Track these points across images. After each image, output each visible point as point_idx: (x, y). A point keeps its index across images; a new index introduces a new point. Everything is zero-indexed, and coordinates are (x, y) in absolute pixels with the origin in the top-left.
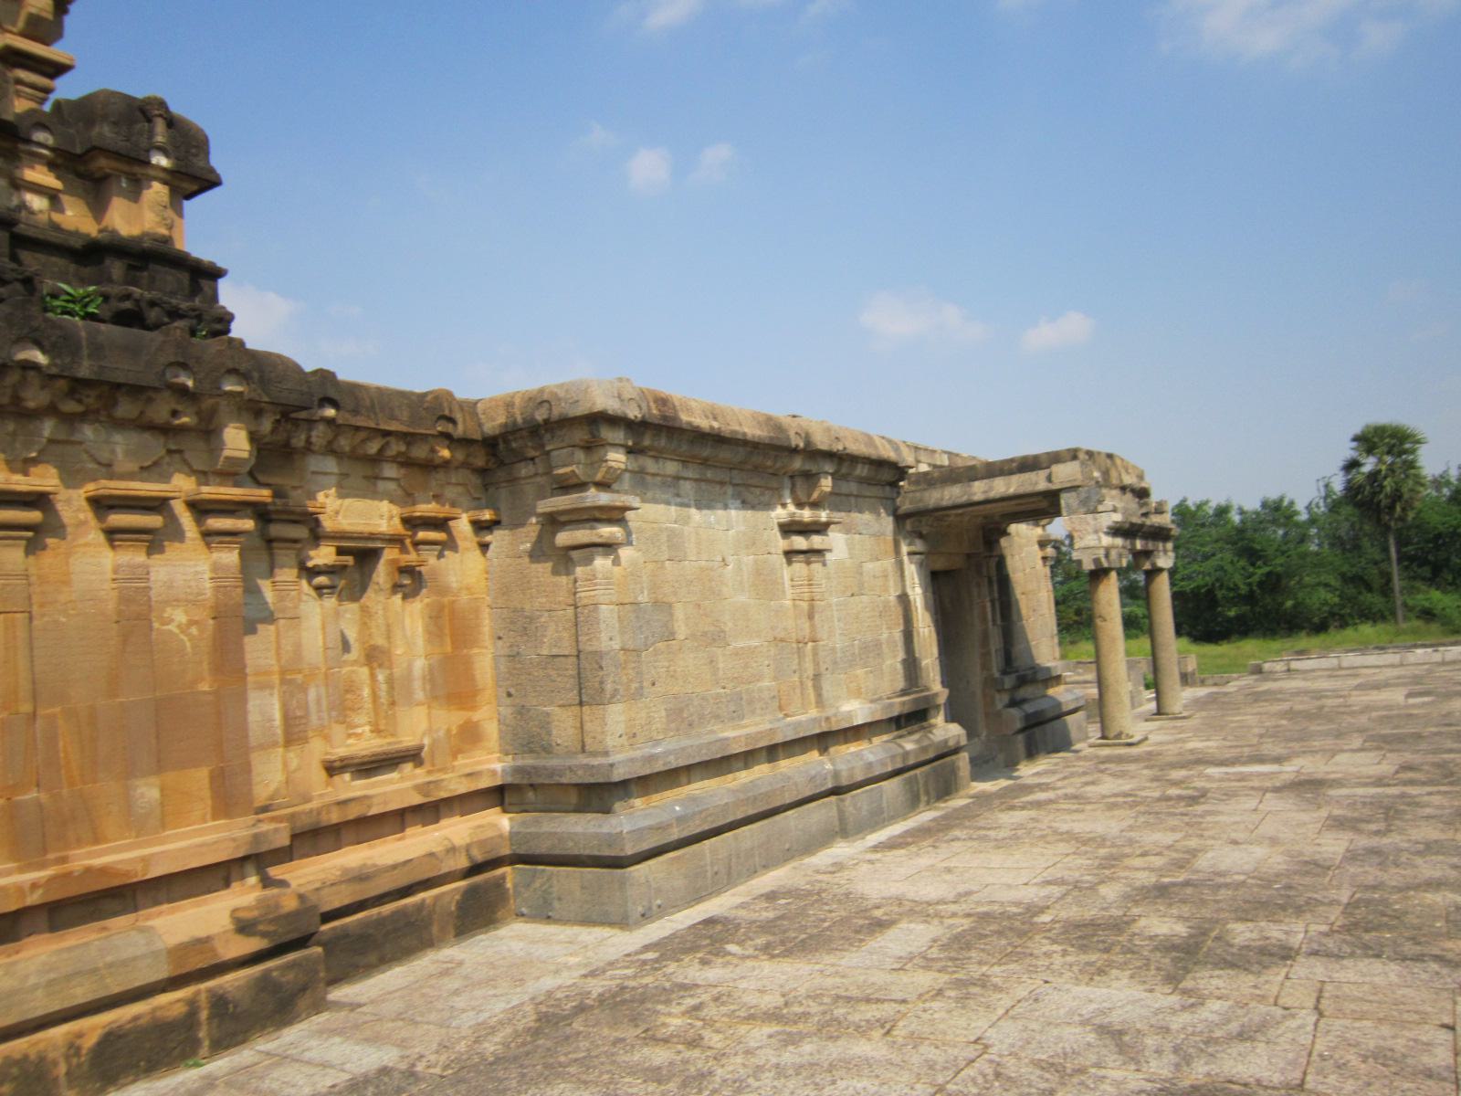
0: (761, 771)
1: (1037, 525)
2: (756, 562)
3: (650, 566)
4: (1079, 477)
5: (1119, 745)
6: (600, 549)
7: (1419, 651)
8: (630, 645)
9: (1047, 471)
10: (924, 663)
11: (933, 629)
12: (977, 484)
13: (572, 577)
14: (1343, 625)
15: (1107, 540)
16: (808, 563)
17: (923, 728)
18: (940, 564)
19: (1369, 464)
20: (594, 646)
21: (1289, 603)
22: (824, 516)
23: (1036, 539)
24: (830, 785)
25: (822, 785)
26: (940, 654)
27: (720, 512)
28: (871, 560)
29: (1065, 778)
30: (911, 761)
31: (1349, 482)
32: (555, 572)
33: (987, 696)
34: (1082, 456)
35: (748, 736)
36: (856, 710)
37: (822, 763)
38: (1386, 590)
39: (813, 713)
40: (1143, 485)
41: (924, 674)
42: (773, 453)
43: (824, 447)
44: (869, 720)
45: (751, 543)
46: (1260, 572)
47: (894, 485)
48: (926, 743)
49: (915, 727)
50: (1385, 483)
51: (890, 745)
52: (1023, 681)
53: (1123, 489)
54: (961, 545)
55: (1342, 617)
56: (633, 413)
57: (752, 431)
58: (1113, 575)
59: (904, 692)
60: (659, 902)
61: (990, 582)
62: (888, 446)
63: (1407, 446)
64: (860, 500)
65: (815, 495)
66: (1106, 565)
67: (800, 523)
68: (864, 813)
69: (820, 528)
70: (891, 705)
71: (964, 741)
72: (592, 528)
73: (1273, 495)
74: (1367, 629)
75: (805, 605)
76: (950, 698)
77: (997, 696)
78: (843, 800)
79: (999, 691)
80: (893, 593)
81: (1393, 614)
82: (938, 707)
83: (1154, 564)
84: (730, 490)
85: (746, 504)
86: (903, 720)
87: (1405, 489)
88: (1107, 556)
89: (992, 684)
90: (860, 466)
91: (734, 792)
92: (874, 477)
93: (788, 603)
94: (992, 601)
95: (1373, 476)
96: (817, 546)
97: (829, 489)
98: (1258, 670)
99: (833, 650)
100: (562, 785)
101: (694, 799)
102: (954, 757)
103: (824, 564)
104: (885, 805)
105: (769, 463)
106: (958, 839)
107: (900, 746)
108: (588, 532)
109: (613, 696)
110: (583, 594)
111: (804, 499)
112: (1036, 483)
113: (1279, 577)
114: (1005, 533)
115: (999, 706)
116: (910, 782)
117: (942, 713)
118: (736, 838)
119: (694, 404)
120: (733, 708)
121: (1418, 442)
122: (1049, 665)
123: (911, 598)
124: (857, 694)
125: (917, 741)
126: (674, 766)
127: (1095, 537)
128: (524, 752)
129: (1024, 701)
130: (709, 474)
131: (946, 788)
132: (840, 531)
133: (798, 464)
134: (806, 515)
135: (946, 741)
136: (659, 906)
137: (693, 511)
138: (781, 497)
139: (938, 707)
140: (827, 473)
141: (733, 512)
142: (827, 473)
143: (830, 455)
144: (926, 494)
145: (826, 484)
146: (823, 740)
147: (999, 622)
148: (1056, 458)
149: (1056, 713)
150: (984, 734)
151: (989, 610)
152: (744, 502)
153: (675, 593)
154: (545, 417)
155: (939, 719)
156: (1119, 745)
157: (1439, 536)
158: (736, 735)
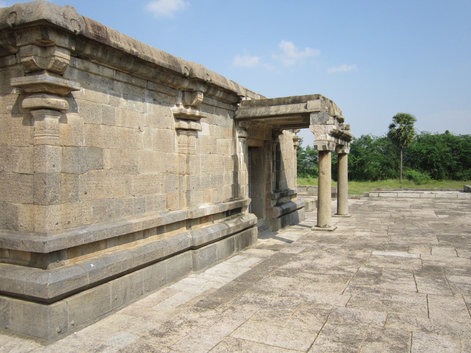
0: (153, 239)
1: (293, 132)
2: (159, 132)
3: (88, 126)
4: (320, 107)
5: (325, 230)
6: (49, 111)
7: (426, 192)
8: (71, 170)
9: (305, 104)
10: (241, 187)
11: (247, 172)
12: (272, 107)
13: (33, 127)
14: (383, 179)
15: (329, 138)
16: (188, 136)
17: (239, 216)
18: (253, 144)
19: (398, 126)
20: (42, 170)
21: (366, 171)
22: (197, 113)
23: (292, 138)
24: (189, 246)
25: (185, 246)
26: (249, 182)
27: (139, 103)
28: (221, 138)
29: (304, 251)
30: (232, 232)
31: (390, 132)
32: (25, 124)
33: (267, 195)
34: (321, 98)
35: (144, 222)
36: (207, 208)
37: (186, 234)
38: (397, 168)
39: (185, 209)
40: (342, 117)
41: (241, 191)
42: (173, 76)
43: (200, 77)
44: (213, 213)
45: (158, 121)
46: (358, 160)
47: (235, 104)
48: (239, 223)
49: (235, 215)
50: (402, 133)
51: (223, 224)
52: (282, 196)
53: (335, 117)
54: (263, 135)
55: (382, 176)
56: (73, 27)
57: (158, 60)
58: (330, 154)
59: (231, 200)
60: (73, 322)
61: (273, 153)
62: (233, 85)
63: (410, 121)
64: (218, 109)
65: (194, 102)
66: (328, 149)
67: (184, 114)
68: (206, 258)
69: (196, 119)
70: (224, 206)
71: (256, 222)
72: (43, 97)
73: (365, 134)
74: (390, 181)
75: (185, 156)
76: (252, 203)
77: (272, 202)
78: (195, 253)
79: (272, 200)
80: (230, 154)
81: (400, 177)
82: (246, 207)
83: (343, 151)
84: (147, 92)
85: (155, 101)
86: (230, 213)
87: (408, 136)
88: (328, 145)
89: (270, 196)
90: (219, 92)
91: (132, 252)
92: (227, 99)
93: (176, 154)
94: (273, 162)
95: (399, 130)
96: (193, 127)
97: (201, 100)
98: (367, 196)
99: (198, 179)
100: (18, 251)
101: (105, 258)
102: (251, 229)
103: (197, 137)
104: (217, 253)
105: (169, 81)
106: (246, 302)
107: (227, 225)
108: (40, 99)
109: (52, 201)
110: (37, 138)
111: (189, 103)
112: (300, 109)
113: (364, 161)
114: (281, 133)
115: (272, 206)
116: (230, 242)
117: (248, 209)
118: (131, 278)
119: (121, 36)
120: (139, 207)
121: (414, 120)
122: (292, 189)
123: (238, 157)
124: (209, 200)
125: (235, 223)
126: (93, 240)
127: (324, 136)
128: (4, 228)
129: (282, 204)
130: (134, 81)
131: (246, 243)
132: (206, 122)
133: (186, 84)
134: (189, 111)
135: (248, 222)
136: (73, 325)
137: (122, 99)
138: (176, 100)
139: (246, 207)
140: (202, 92)
141: (148, 104)
142: (202, 92)
143: (203, 83)
144: (249, 110)
145: (200, 97)
146: (189, 222)
147: (275, 170)
148: (309, 98)
149: (294, 209)
150: (265, 217)
151: (271, 165)
152: (154, 100)
153: (105, 143)
154: (13, 22)
155: (246, 212)
156: (325, 230)
157: (415, 152)
158: (137, 222)
